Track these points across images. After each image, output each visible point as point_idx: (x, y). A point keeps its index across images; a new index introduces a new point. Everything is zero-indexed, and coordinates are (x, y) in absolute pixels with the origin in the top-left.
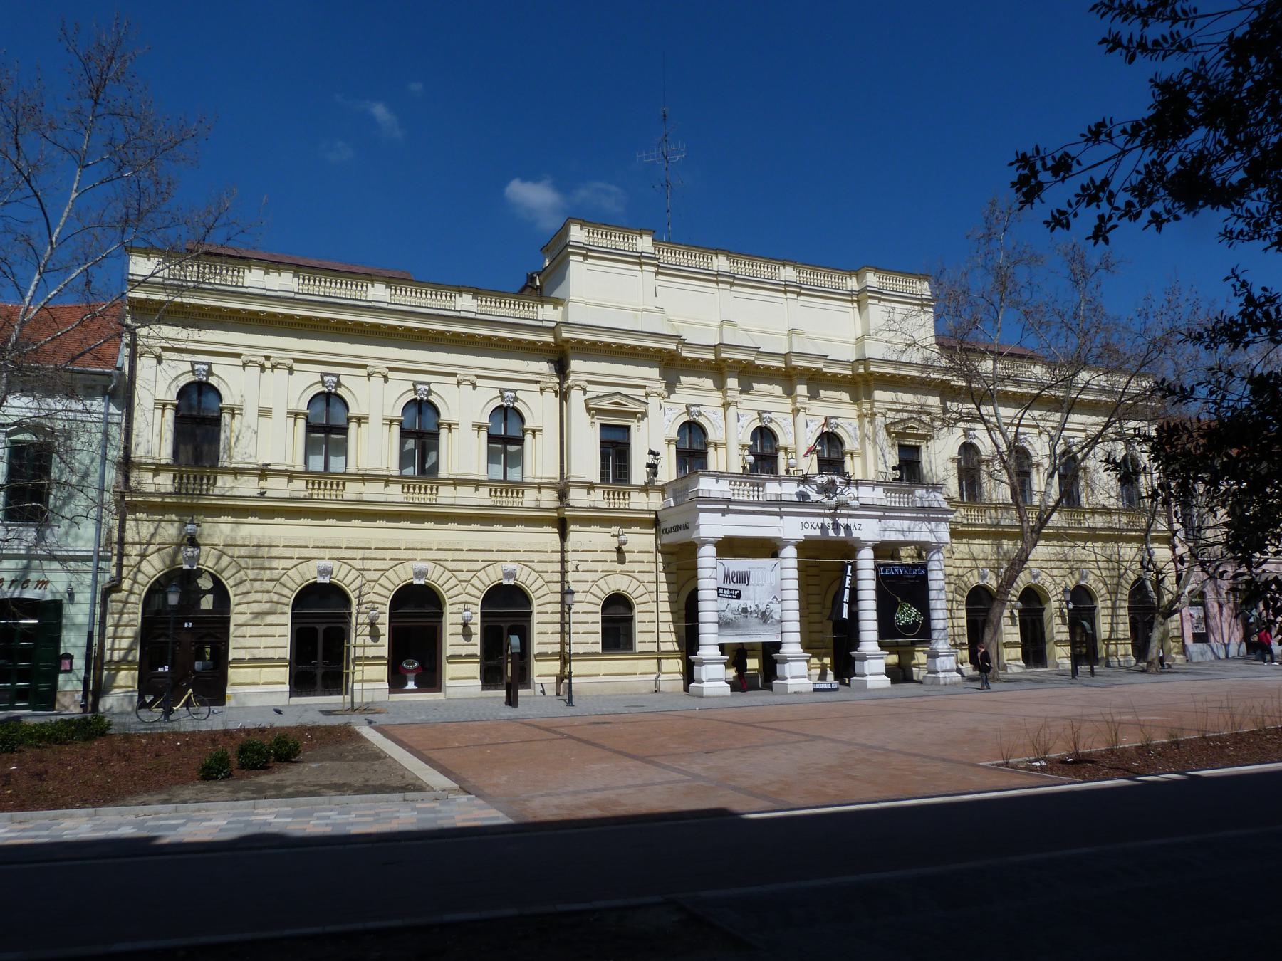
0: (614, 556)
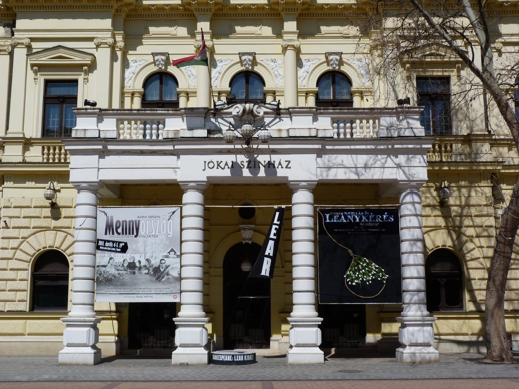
0: (47, 212)
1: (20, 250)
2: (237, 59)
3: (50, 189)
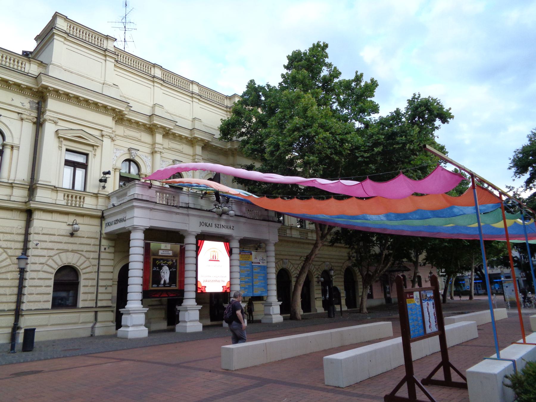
1: (47, 265)
2: (171, 162)
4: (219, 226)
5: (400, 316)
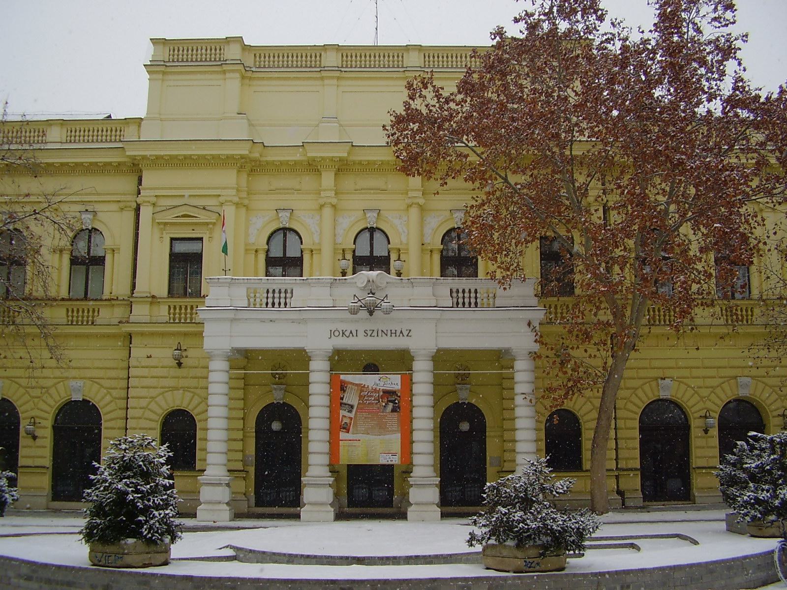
1: (149, 409)
2: (448, 213)
3: (177, 349)
4: (375, 334)
5: (441, 481)
